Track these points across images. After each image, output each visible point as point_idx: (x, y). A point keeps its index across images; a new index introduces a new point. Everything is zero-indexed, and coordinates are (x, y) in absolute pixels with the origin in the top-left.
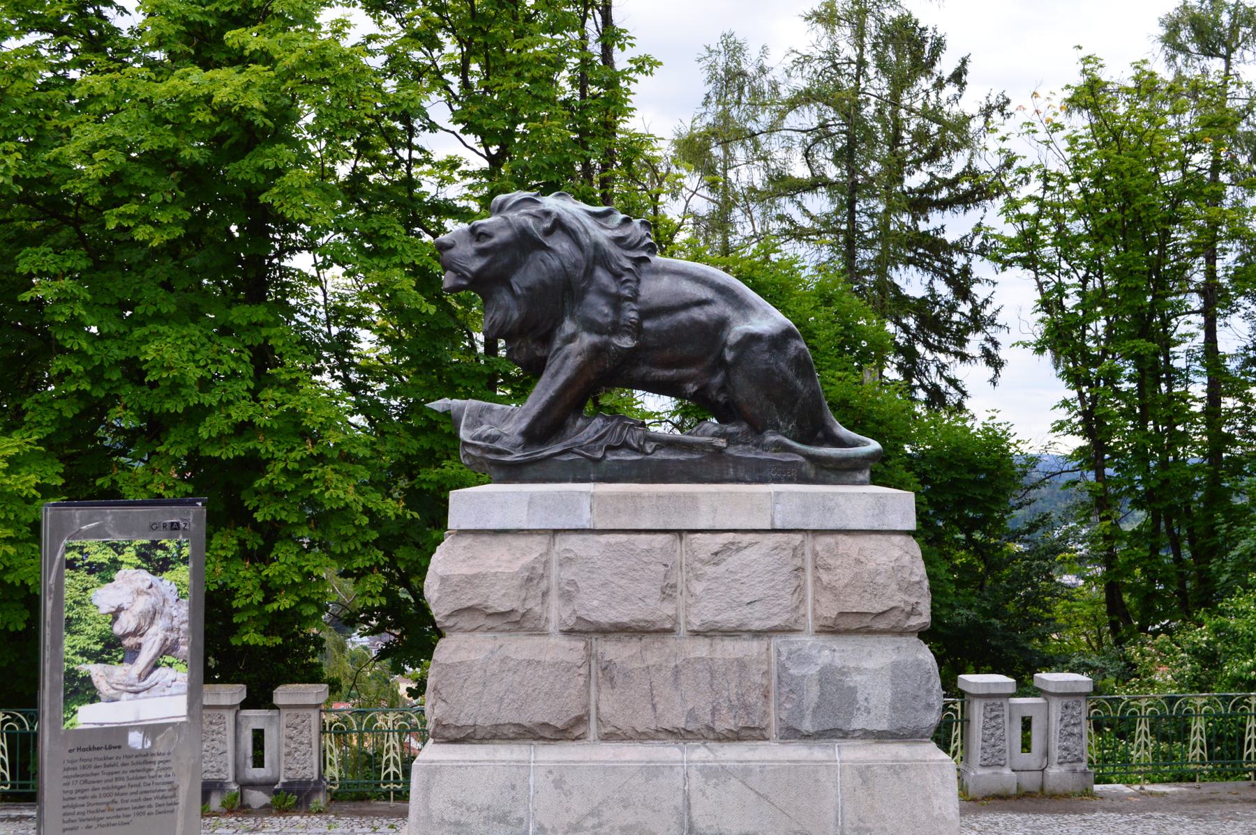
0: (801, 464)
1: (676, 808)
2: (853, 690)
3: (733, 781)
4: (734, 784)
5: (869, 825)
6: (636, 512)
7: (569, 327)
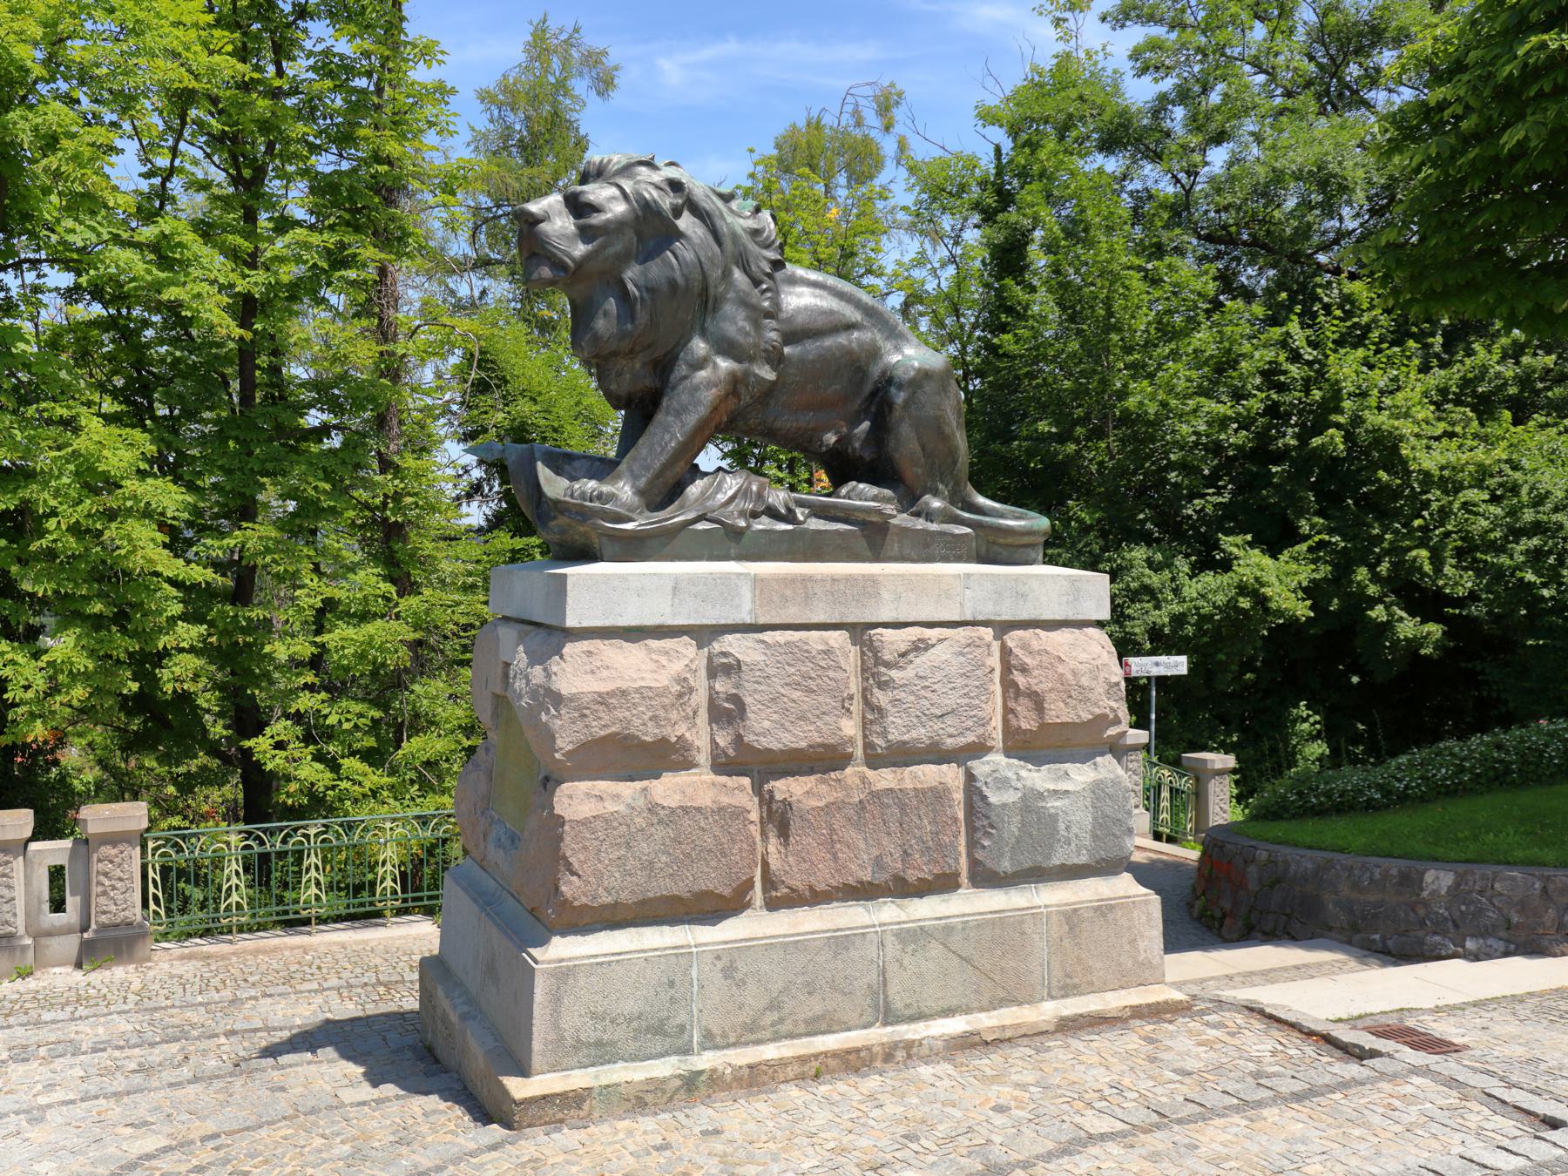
1: (869, 986)
2: (1054, 818)
3: (934, 944)
4: (935, 949)
5: (1076, 980)
6: (808, 599)
7: (699, 346)
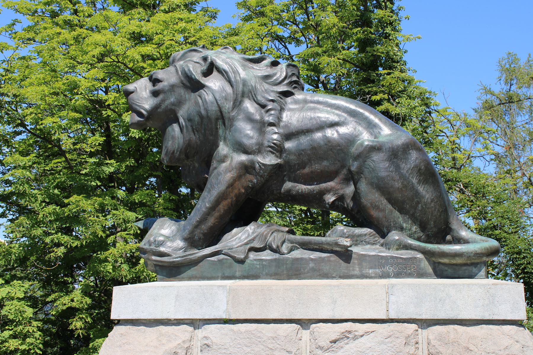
0: (420, 260)
7: (223, 149)
